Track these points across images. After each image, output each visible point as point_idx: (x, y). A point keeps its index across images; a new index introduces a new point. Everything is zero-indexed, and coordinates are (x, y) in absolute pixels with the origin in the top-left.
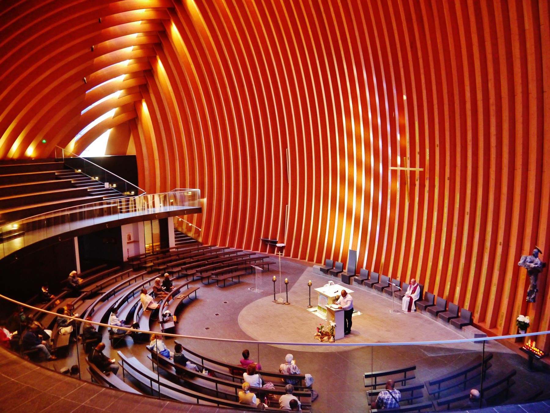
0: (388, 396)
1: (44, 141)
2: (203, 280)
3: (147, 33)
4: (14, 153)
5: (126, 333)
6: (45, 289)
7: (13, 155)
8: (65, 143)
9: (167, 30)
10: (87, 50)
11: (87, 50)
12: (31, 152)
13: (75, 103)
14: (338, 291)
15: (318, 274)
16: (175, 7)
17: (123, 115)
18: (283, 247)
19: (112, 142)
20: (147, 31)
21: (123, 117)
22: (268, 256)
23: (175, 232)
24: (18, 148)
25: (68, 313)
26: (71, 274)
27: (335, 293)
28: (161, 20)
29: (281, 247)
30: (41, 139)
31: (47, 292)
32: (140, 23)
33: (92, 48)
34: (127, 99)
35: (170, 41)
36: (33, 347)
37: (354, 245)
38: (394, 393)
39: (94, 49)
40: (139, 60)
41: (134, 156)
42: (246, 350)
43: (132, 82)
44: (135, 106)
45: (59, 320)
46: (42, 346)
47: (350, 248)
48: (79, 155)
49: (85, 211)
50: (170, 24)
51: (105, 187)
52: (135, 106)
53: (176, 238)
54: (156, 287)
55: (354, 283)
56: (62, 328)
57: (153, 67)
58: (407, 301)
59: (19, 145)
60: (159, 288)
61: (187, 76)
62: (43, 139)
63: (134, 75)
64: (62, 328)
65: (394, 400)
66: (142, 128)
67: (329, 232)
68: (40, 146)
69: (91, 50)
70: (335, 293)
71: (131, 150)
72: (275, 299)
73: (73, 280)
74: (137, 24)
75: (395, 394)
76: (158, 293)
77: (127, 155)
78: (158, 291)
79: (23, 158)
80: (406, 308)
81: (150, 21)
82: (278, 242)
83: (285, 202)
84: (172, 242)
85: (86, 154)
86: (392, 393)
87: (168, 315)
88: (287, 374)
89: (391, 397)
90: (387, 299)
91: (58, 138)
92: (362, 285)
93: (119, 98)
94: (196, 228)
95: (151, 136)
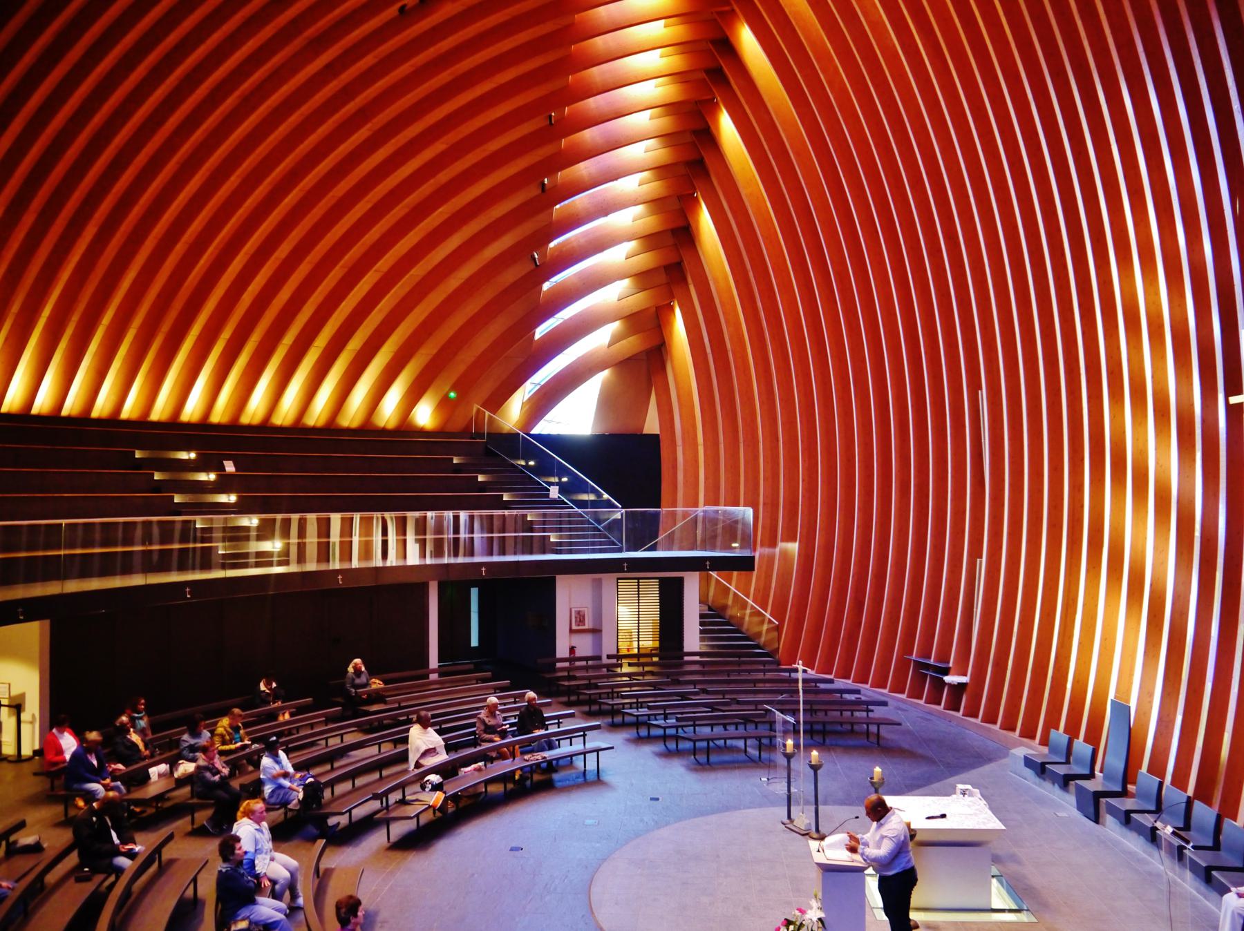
1: (452, 395)
2: (639, 727)
3: (667, 138)
5: (289, 804)
6: (268, 684)
8: (498, 400)
10: (532, 191)
11: (532, 191)
12: (425, 415)
13: (517, 310)
14: (943, 816)
15: (1019, 776)
16: (721, 67)
18: (961, 687)
19: (608, 402)
21: (632, 344)
22: (883, 699)
23: (700, 618)
24: (397, 407)
25: (225, 732)
27: (928, 818)
28: (696, 102)
29: (954, 685)
30: (447, 389)
31: (268, 691)
32: (648, 117)
33: (543, 184)
34: (639, 300)
36: (76, 786)
37: (1146, 693)
39: (547, 188)
40: (657, 204)
42: (351, 897)
43: (645, 260)
44: (658, 317)
45: (184, 741)
46: (96, 789)
47: (1111, 695)
49: (515, 553)
51: (551, 496)
52: (658, 317)
53: (702, 632)
55: (1109, 819)
56: (183, 763)
59: (401, 400)
60: (489, 724)
61: (344, 110)
63: (651, 241)
64: (183, 763)
66: (673, 368)
67: (1080, 643)
69: (539, 191)
70: (928, 818)
71: (652, 425)
72: (789, 817)
73: (353, 680)
76: (484, 735)
77: (644, 433)
78: (485, 732)
79: (405, 432)
81: (670, 108)
82: (952, 671)
84: (693, 640)
85: (547, 426)
87: (430, 786)
90: (1197, 895)
91: (486, 388)
93: (619, 300)
95: (691, 386)
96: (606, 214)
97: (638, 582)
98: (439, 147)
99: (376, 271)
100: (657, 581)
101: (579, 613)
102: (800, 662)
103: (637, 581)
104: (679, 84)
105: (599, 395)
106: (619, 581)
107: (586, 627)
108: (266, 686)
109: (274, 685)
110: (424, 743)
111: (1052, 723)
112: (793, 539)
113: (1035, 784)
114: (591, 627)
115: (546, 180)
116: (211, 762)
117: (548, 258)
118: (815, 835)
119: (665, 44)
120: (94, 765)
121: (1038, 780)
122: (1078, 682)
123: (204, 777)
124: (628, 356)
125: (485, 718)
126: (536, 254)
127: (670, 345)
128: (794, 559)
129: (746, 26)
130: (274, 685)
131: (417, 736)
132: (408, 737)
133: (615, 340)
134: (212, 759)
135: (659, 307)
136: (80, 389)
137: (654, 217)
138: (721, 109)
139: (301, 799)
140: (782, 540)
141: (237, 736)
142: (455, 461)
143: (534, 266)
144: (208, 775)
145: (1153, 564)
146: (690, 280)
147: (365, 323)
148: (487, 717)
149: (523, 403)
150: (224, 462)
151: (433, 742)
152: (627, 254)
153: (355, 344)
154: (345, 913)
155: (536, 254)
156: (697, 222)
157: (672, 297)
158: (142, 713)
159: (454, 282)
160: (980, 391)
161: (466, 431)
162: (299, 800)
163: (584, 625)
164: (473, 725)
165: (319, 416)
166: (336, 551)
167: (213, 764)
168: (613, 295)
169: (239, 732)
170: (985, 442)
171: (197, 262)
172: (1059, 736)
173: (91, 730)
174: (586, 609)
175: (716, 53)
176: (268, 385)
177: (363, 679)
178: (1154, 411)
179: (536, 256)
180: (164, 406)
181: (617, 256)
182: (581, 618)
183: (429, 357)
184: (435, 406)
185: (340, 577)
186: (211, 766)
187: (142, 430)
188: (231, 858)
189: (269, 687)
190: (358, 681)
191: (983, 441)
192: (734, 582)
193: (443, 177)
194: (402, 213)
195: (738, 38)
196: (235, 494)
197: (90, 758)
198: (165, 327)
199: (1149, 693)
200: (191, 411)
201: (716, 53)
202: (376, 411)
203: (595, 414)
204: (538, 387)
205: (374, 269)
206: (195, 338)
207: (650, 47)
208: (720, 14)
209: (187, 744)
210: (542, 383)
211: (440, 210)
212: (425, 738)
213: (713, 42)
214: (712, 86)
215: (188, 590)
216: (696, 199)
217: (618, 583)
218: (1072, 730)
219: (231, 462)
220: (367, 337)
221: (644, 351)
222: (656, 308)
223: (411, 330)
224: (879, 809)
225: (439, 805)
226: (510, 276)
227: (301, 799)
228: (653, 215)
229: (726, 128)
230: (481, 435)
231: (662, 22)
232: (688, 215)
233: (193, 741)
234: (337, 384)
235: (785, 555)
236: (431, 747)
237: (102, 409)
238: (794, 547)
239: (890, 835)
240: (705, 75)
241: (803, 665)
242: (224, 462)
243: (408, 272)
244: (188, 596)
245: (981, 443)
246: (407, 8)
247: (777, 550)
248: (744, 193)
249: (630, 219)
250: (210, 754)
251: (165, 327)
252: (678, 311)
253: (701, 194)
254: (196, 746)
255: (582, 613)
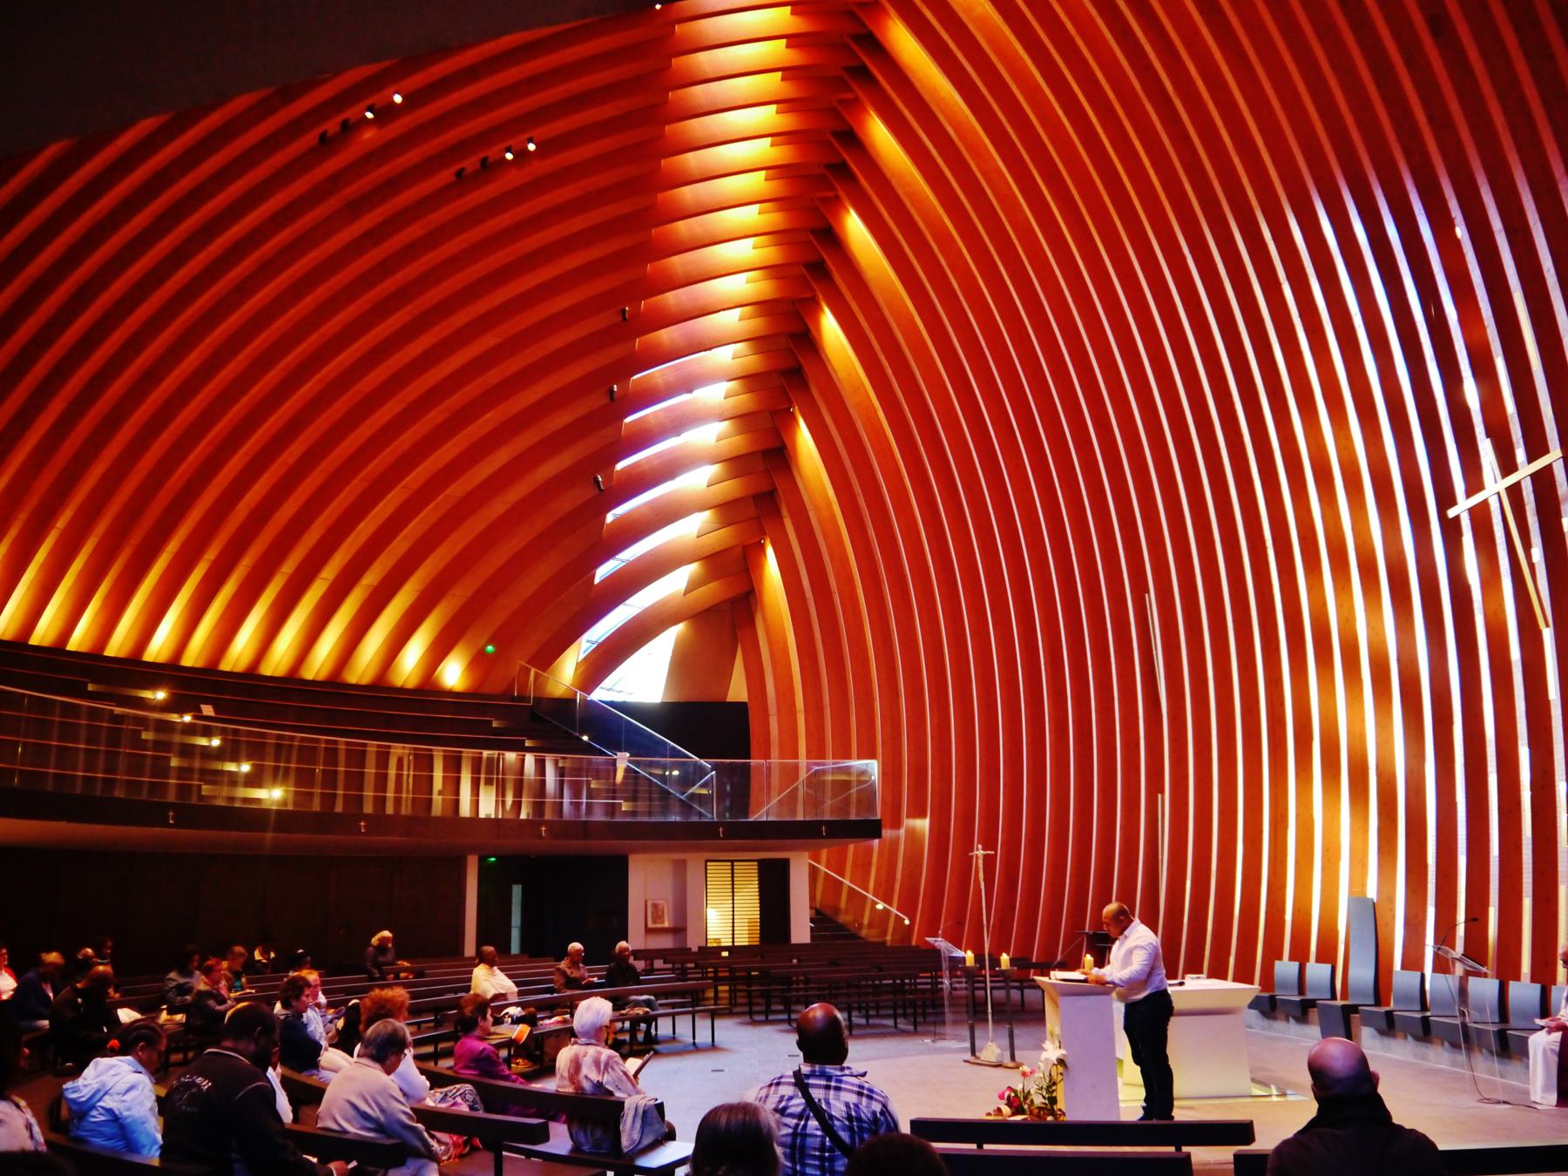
0: (782, 1097)
1: (490, 649)
3: (759, 342)
4: (409, 675)
6: (265, 953)
7: (405, 681)
8: (548, 655)
9: (811, 327)
10: (597, 401)
11: (597, 401)
12: (454, 674)
16: (823, 260)
17: (713, 586)
19: (682, 664)
20: (757, 335)
21: (711, 592)
26: (375, 941)
30: (483, 641)
31: (264, 961)
34: (722, 537)
35: (823, 356)
36: (23, 1024)
38: (823, 1082)
39: (616, 396)
40: (744, 420)
41: (744, 705)
43: (730, 488)
44: (745, 558)
45: (171, 979)
48: (589, 694)
50: (815, 310)
52: (745, 558)
54: (565, 971)
57: (785, 438)
58: (1545, 1050)
60: (572, 976)
62: (488, 643)
63: (737, 464)
65: (813, 1123)
66: (765, 619)
67: (1297, 862)
68: (478, 662)
71: (738, 690)
74: (730, 320)
75: (828, 1088)
79: (428, 691)
80: (1546, 1089)
81: (763, 307)
83: (1155, 786)
86: (811, 1081)
87: (510, 1020)
88: (566, 1090)
89: (798, 1104)
91: (532, 644)
92: (1394, 1036)
94: (843, 877)
96: (365, 1113)
97: (733, 866)
98: (489, 341)
99: (404, 487)
100: (756, 863)
101: (655, 906)
102: (980, 846)
103: (730, 864)
104: (773, 281)
105: (672, 657)
106: (708, 864)
107: (666, 925)
108: (262, 954)
109: (272, 955)
110: (493, 986)
111: (1273, 952)
112: (922, 815)
113: (1263, 1029)
114: (672, 926)
115: (615, 386)
116: (216, 987)
117: (614, 483)
118: (1012, 1064)
119: (760, 232)
120: (49, 997)
121: (1266, 1022)
122: (1299, 910)
123: (207, 1006)
124: (707, 607)
125: (566, 969)
126: (599, 477)
127: (761, 592)
128: (924, 843)
129: (852, 212)
130: (272, 955)
131: (484, 977)
132: (471, 978)
133: (693, 586)
134: (218, 982)
135: (746, 546)
136: (17, 608)
137: (742, 436)
138: (822, 310)
139: (340, 1029)
140: (908, 817)
141: (238, 984)
142: (494, 725)
143: (597, 491)
144: (211, 1003)
145: (1377, 743)
146: (785, 512)
147: (387, 551)
148: (569, 968)
149: (577, 664)
150: (202, 706)
151: (504, 986)
152: (709, 480)
153: (370, 579)
154: (472, 1012)
155: (599, 477)
156: (794, 442)
157: (763, 534)
158: (106, 959)
159: (500, 506)
160: (1147, 595)
161: (507, 695)
162: (337, 1030)
163: (663, 922)
164: (551, 973)
165: (320, 668)
166: (371, 760)
167: (218, 990)
168: (689, 529)
169: (240, 980)
170: (1157, 654)
171: (184, 459)
172: (1285, 968)
173: (49, 951)
174: (662, 902)
175: (818, 247)
176: (258, 626)
177: (390, 957)
178: (1359, 566)
179: (600, 479)
180: (123, 642)
181: (698, 481)
182: (658, 914)
183: (465, 599)
184: (464, 667)
185: (363, 824)
186: (214, 991)
187: (93, 662)
188: (294, 1003)
189: (266, 956)
190: (381, 959)
191: (1154, 652)
192: (848, 872)
193: (493, 377)
194: (441, 419)
195: (842, 225)
196: (220, 737)
197: (45, 987)
198: (135, 539)
199: (1388, 898)
200: (158, 648)
201: (818, 247)
202: (393, 665)
203: (668, 677)
204: (595, 646)
205: (403, 483)
206: (172, 555)
207: (743, 235)
208: (824, 200)
209: (174, 983)
210: (600, 641)
211: (488, 416)
212: (493, 980)
213: (815, 232)
214: (811, 281)
215: (171, 814)
216: (793, 414)
217: (706, 866)
218: (1300, 954)
219: (210, 706)
220: (387, 570)
221: (724, 602)
222: (744, 547)
223: (441, 566)
224: (1122, 917)
225: (524, 1039)
226: (569, 501)
227: (340, 1029)
228: (742, 434)
229: (830, 328)
230: (522, 698)
231: (757, 207)
232: (782, 433)
233: (182, 980)
234: (346, 628)
235: (913, 835)
236: (503, 992)
237: (43, 637)
238: (923, 825)
239: (1143, 944)
240: (803, 270)
241: (983, 849)
242: (202, 706)
243: (443, 491)
244: (171, 822)
245: (1152, 655)
246: (465, 173)
247: (902, 832)
248: (851, 403)
249: (711, 436)
250: (215, 975)
251: (135, 539)
252: (770, 551)
253: (799, 409)
254: (186, 986)
255: (660, 907)
